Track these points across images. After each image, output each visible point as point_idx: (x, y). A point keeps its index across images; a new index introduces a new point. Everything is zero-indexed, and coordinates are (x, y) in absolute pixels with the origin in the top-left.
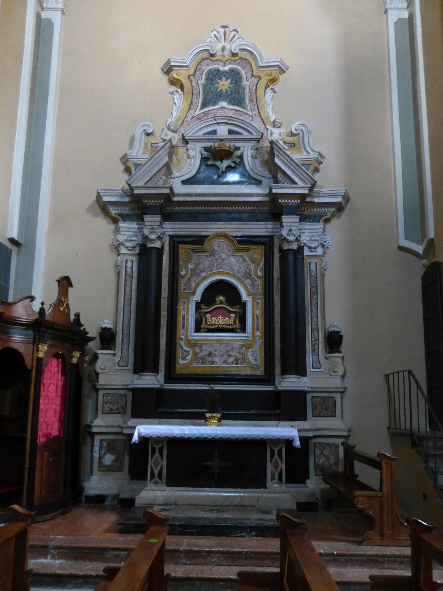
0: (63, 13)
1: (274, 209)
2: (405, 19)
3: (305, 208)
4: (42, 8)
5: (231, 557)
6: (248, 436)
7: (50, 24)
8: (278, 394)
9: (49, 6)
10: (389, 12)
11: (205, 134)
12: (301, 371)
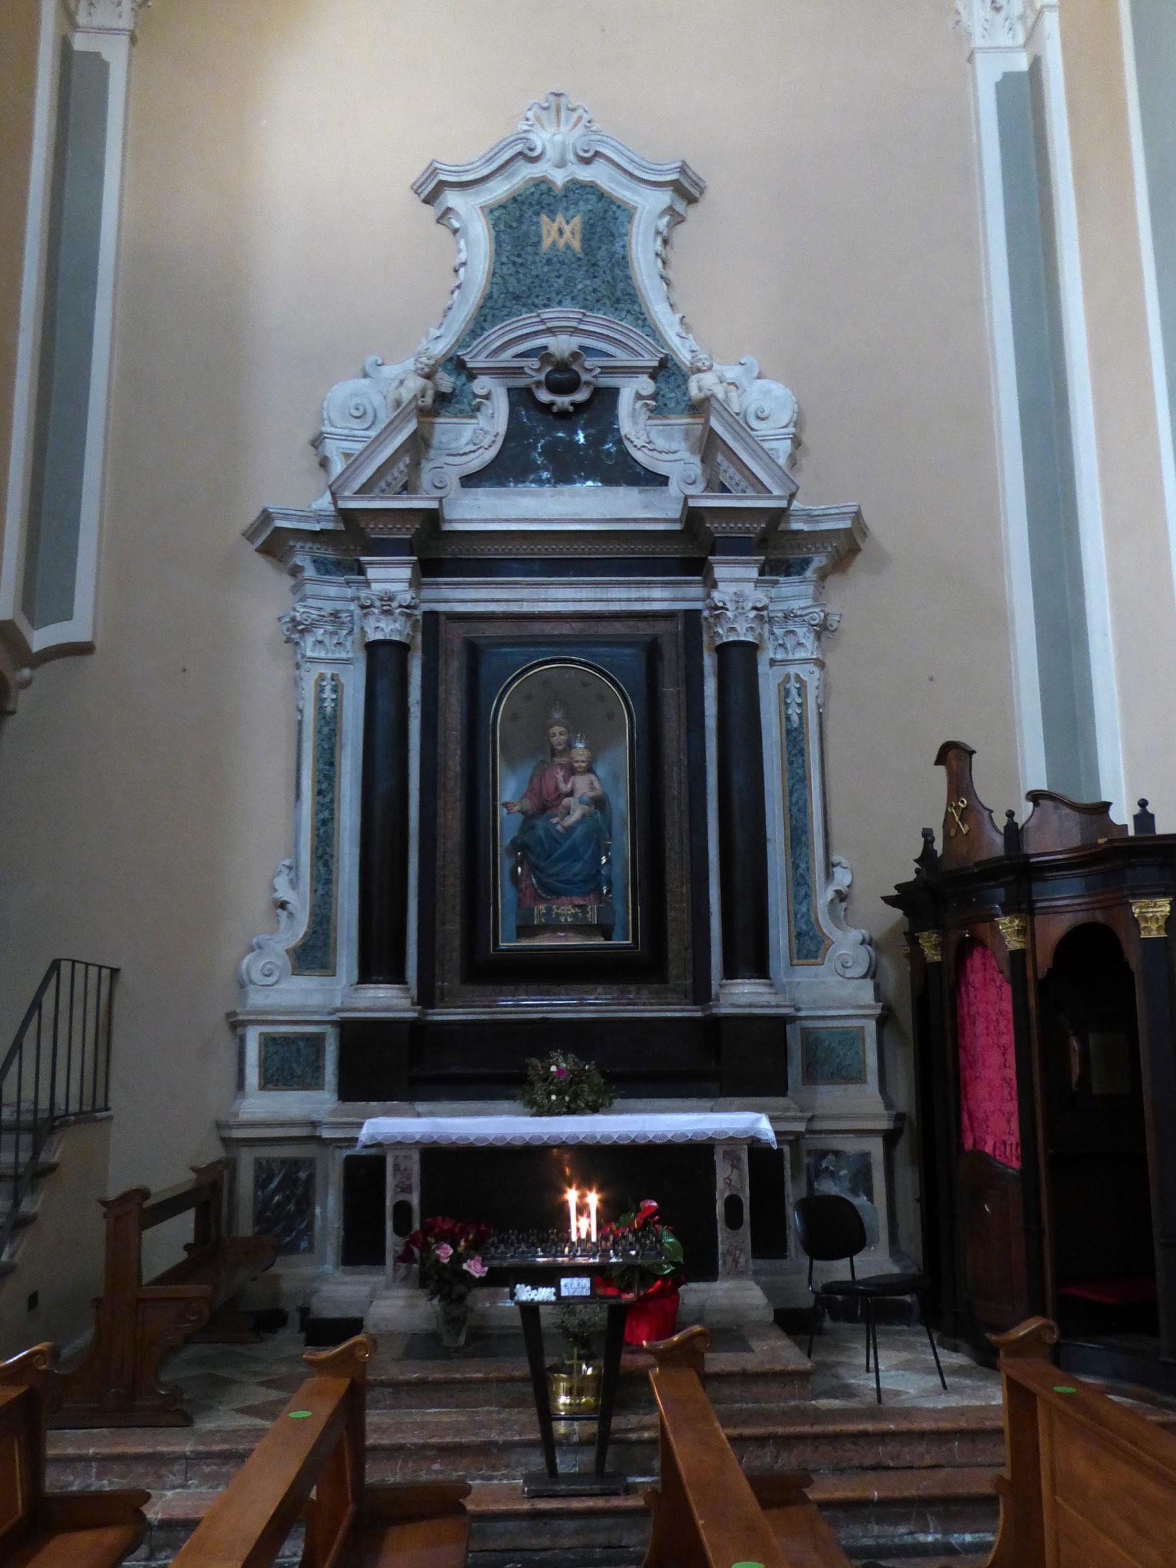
0: (133, 40)
1: (690, 548)
2: (1020, 74)
3: (774, 544)
4: (75, 27)
5: (768, 1417)
6: (695, 1134)
7: (98, 65)
8: (715, 1026)
9: (99, 20)
10: (979, 58)
11: (516, 356)
12: (760, 968)
